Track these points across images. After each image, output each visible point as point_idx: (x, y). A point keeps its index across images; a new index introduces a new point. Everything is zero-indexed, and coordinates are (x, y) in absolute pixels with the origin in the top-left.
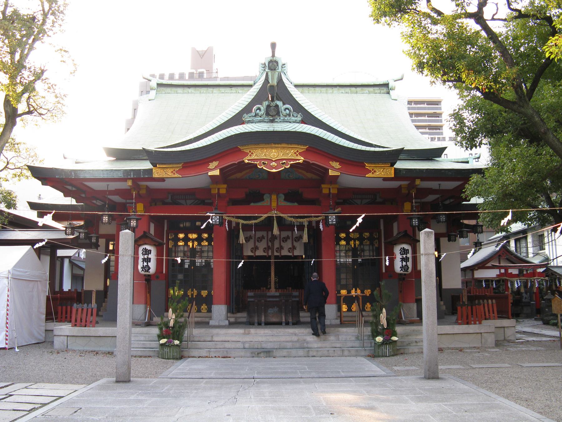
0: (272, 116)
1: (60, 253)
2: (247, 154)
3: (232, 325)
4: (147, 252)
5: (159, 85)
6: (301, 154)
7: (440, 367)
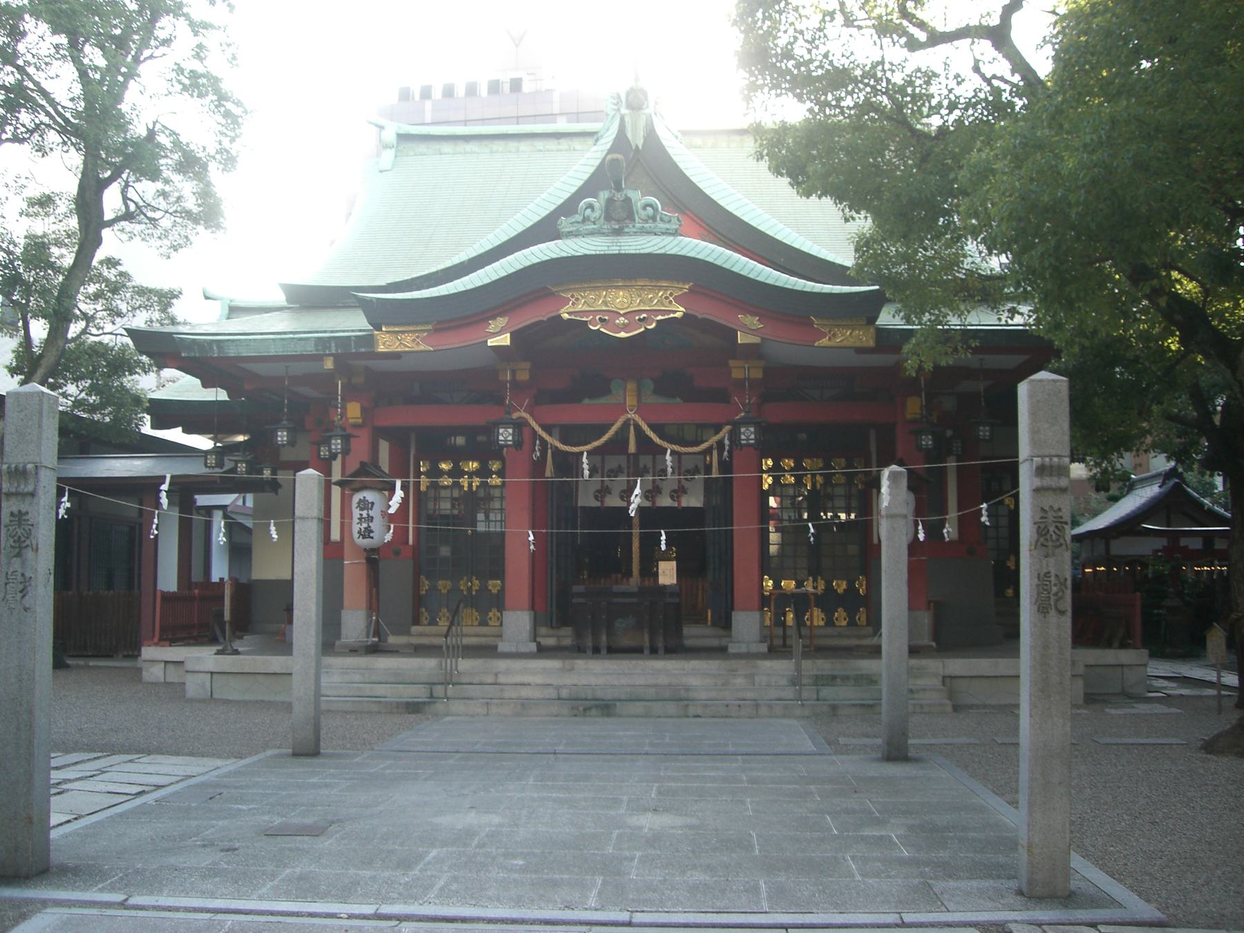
0: (618, 221)
1: (202, 500)
2: (566, 301)
3: (543, 652)
4: (364, 505)
5: (403, 138)
6: (678, 300)
7: (910, 742)
